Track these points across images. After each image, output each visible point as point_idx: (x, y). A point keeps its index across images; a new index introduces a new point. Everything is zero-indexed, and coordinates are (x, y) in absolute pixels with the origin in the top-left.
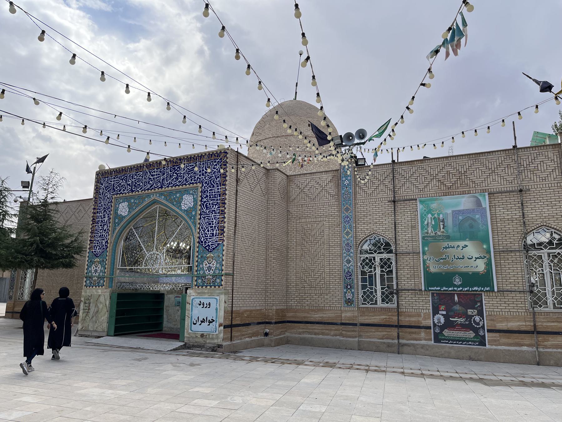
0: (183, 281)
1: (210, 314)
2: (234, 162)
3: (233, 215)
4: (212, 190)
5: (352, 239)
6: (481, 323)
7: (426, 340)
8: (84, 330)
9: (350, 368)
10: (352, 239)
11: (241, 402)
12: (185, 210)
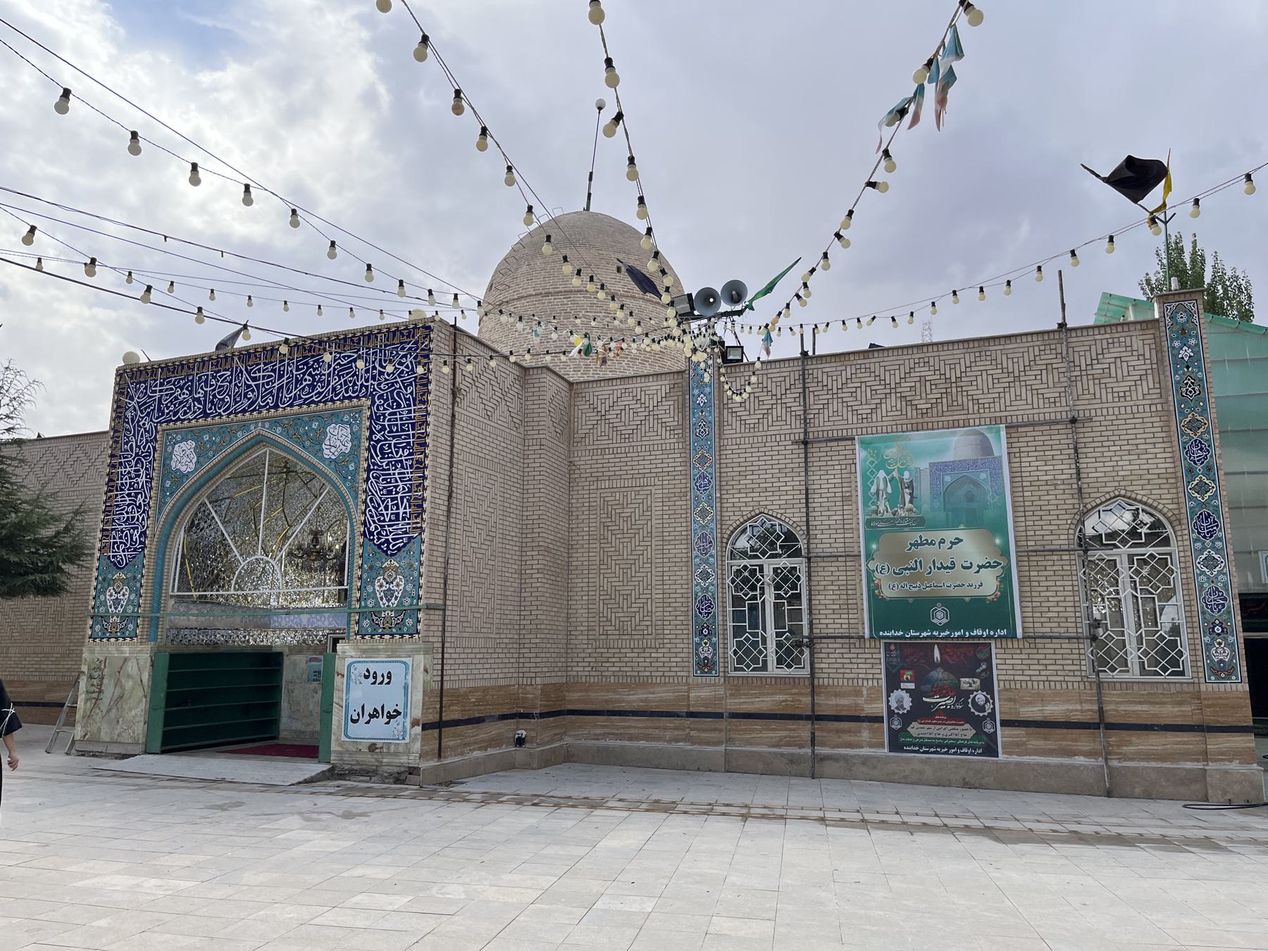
1: (390, 697)
7: (871, 745)
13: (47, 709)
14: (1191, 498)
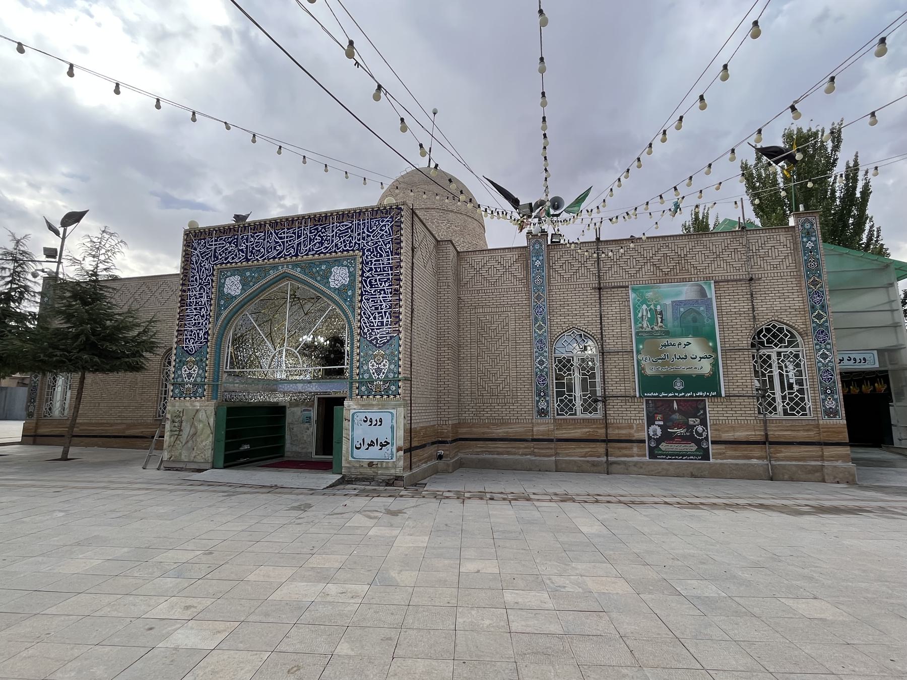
1: (382, 434)
7: (639, 456)
8: (173, 461)
13: (128, 440)
14: (814, 322)
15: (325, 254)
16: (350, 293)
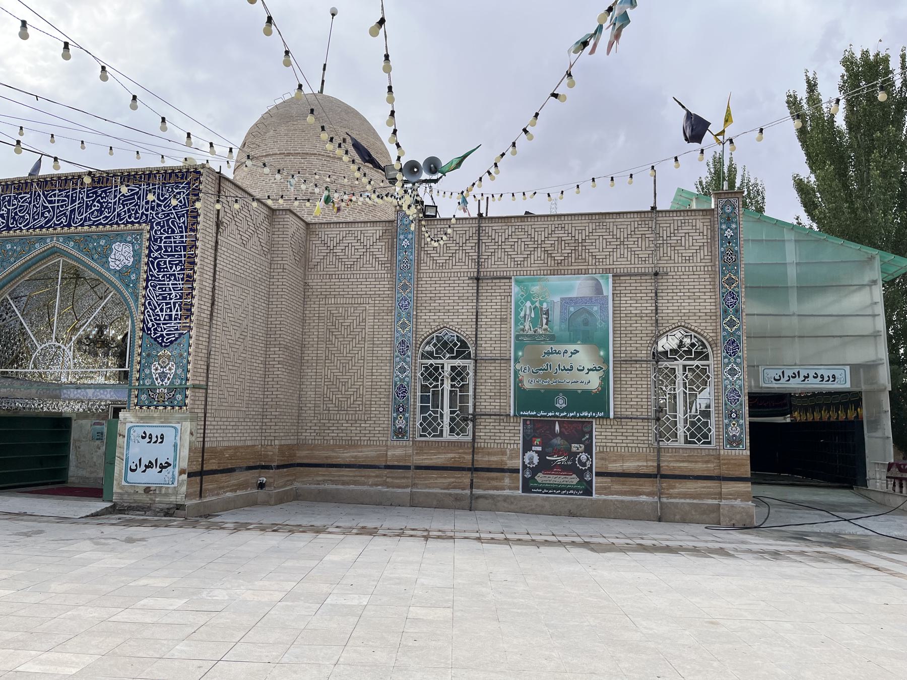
0: (108, 396)
1: (163, 453)
2: (213, 190)
3: (208, 284)
4: (170, 238)
5: (410, 334)
6: (589, 464)
7: (510, 488)
9: (401, 534)
10: (410, 334)
11: (227, 598)
12: (116, 271)
14: (724, 330)
15: (104, 225)
16: (133, 277)
